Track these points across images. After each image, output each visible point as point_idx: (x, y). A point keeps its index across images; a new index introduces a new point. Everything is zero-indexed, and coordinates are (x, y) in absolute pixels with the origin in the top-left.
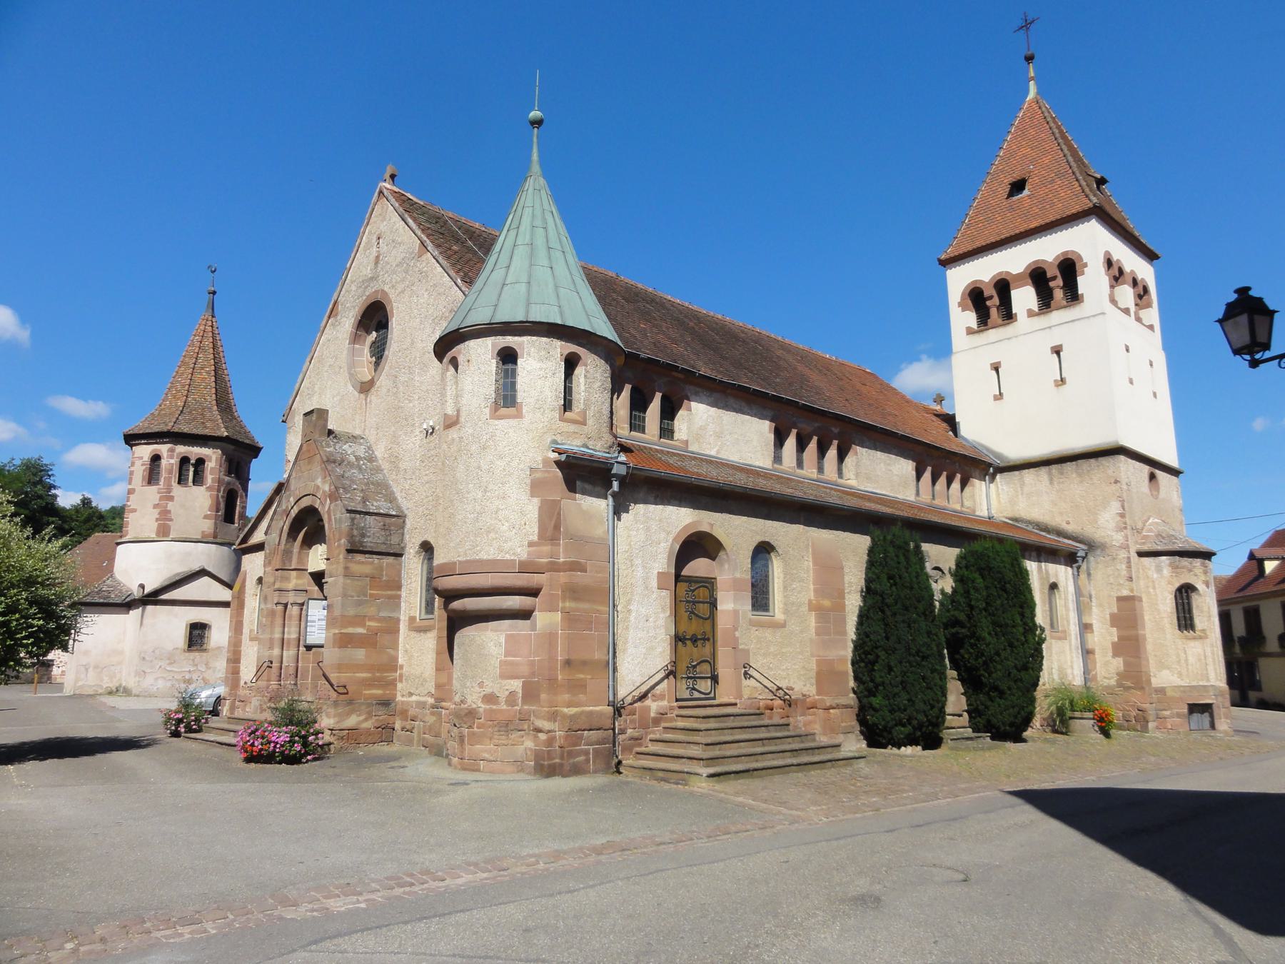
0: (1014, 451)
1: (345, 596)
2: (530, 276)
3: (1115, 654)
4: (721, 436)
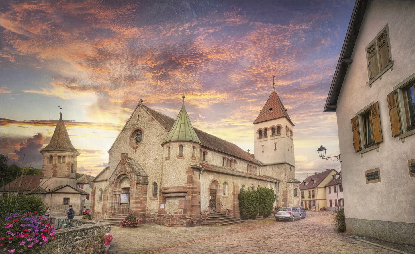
0: (265, 162)
1: (136, 193)
2: (185, 130)
3: (282, 201)
4: (214, 159)
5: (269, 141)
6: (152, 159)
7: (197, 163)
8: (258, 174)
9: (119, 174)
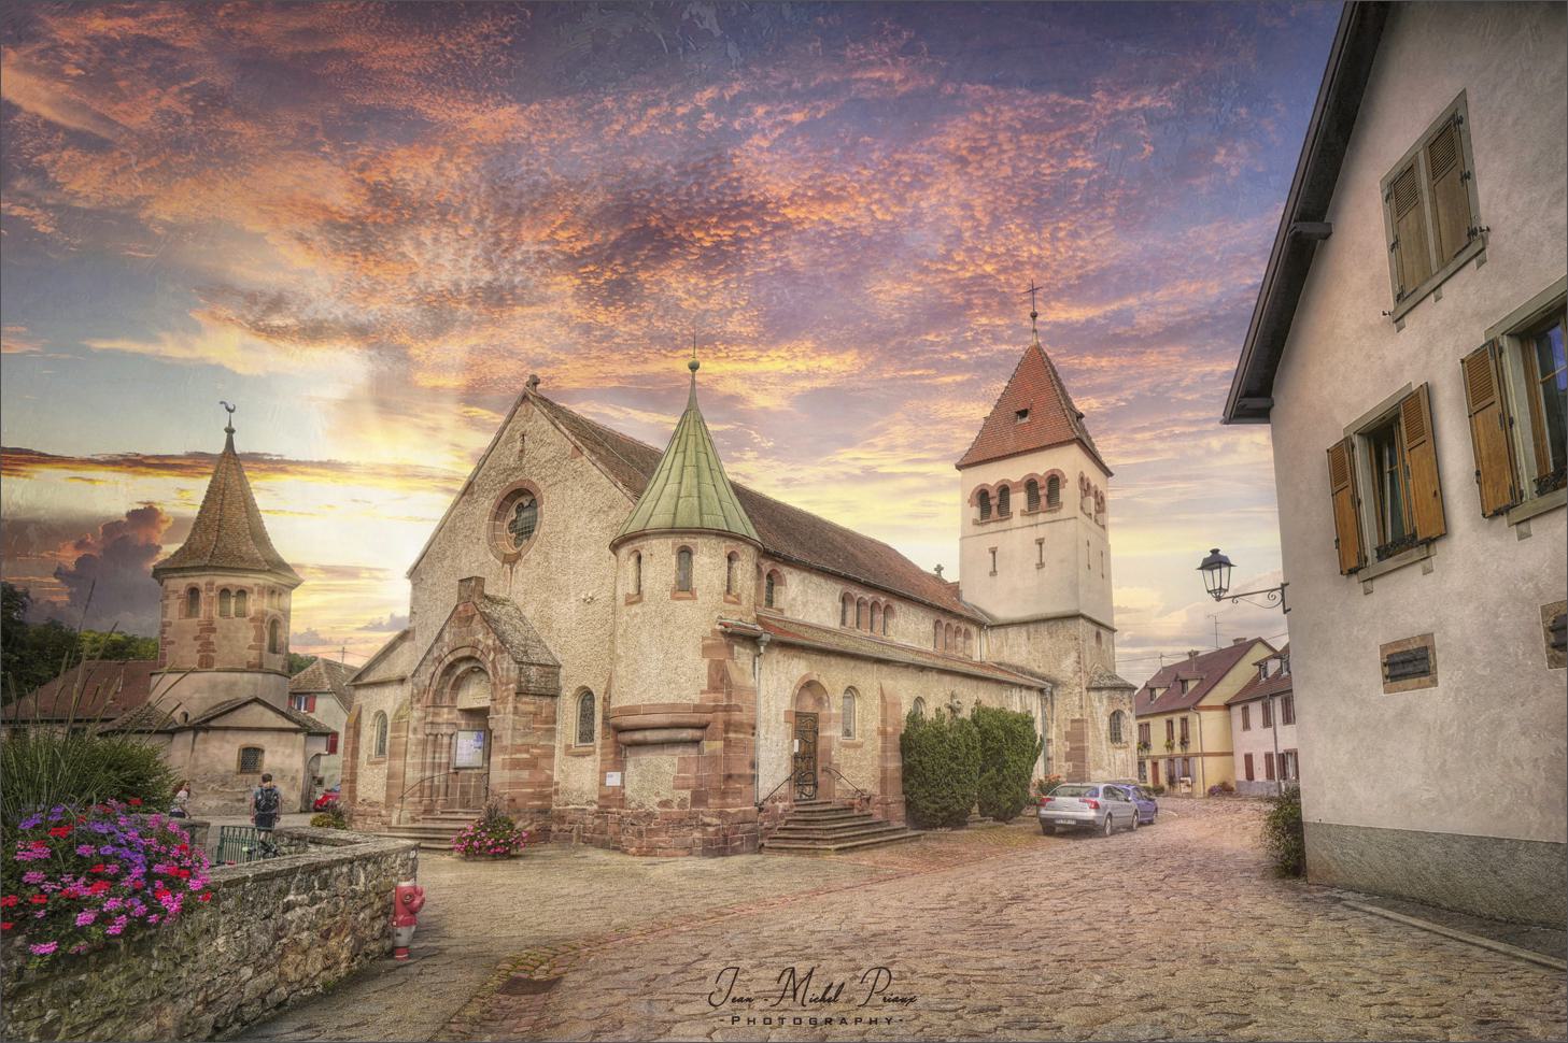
0: (1002, 613)
1: (514, 729)
2: (699, 492)
3: (1067, 761)
4: (810, 602)
5: (1018, 534)
6: (572, 600)
7: (743, 615)
8: (976, 659)
9: (451, 658)
